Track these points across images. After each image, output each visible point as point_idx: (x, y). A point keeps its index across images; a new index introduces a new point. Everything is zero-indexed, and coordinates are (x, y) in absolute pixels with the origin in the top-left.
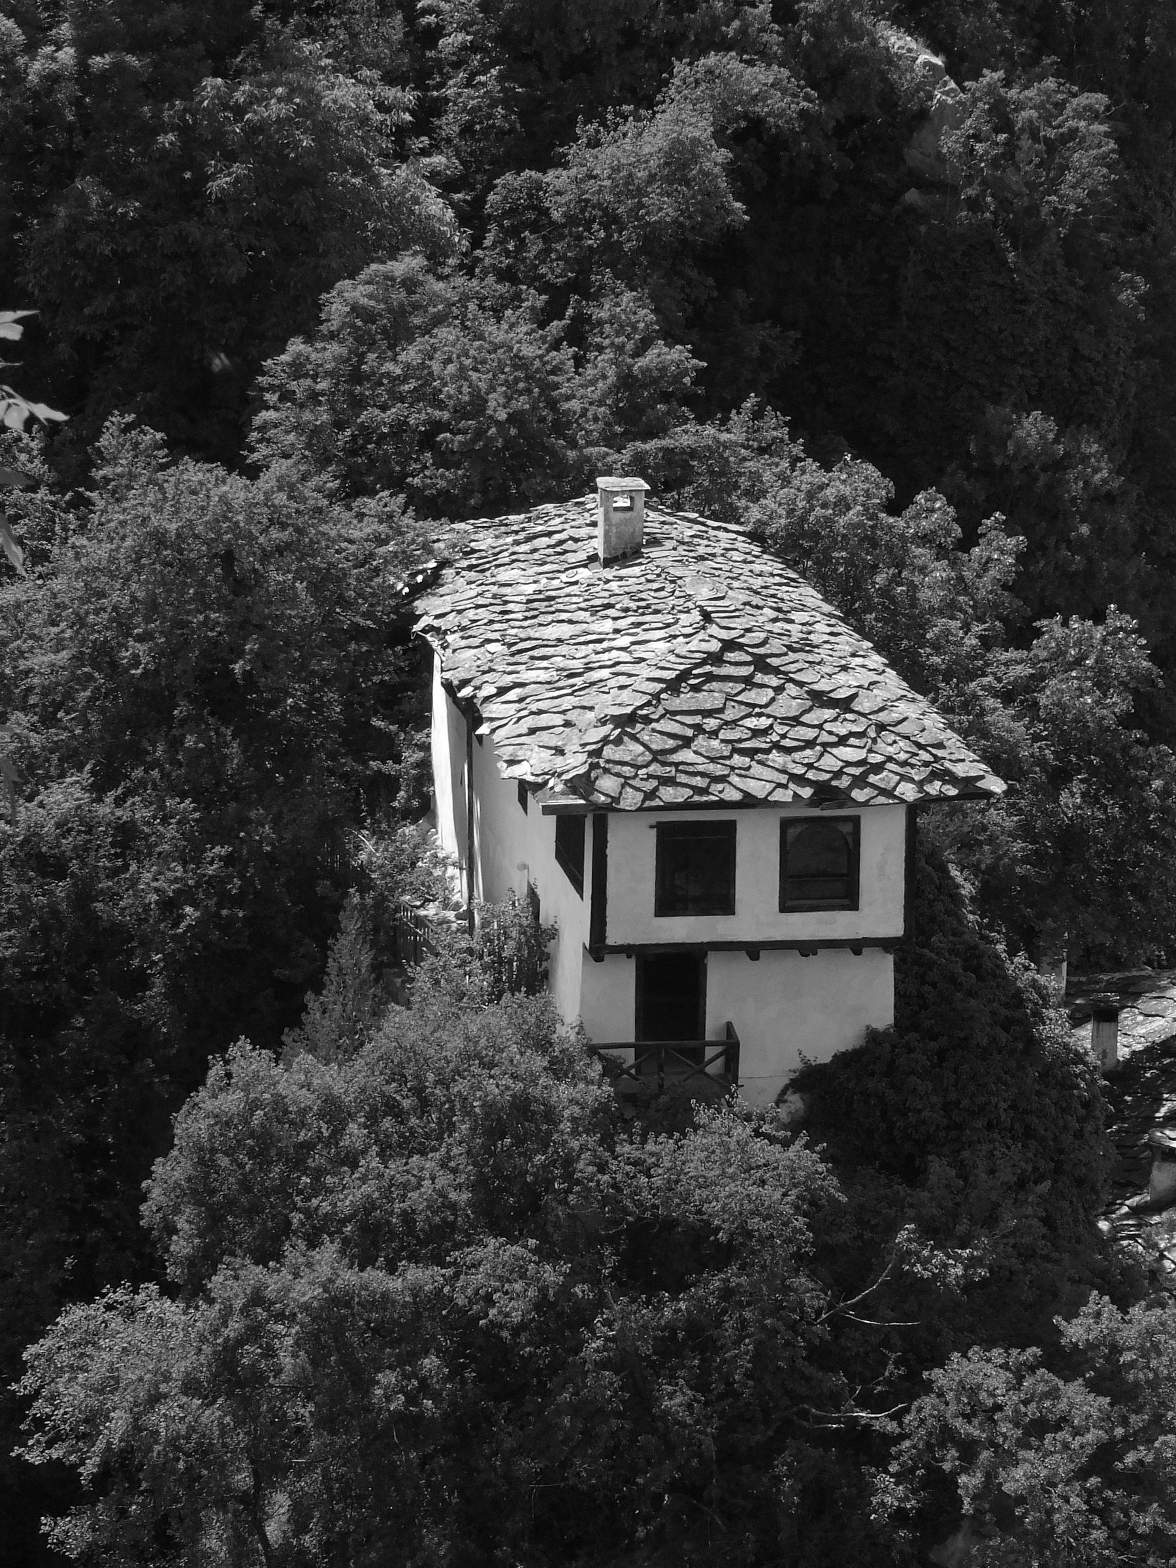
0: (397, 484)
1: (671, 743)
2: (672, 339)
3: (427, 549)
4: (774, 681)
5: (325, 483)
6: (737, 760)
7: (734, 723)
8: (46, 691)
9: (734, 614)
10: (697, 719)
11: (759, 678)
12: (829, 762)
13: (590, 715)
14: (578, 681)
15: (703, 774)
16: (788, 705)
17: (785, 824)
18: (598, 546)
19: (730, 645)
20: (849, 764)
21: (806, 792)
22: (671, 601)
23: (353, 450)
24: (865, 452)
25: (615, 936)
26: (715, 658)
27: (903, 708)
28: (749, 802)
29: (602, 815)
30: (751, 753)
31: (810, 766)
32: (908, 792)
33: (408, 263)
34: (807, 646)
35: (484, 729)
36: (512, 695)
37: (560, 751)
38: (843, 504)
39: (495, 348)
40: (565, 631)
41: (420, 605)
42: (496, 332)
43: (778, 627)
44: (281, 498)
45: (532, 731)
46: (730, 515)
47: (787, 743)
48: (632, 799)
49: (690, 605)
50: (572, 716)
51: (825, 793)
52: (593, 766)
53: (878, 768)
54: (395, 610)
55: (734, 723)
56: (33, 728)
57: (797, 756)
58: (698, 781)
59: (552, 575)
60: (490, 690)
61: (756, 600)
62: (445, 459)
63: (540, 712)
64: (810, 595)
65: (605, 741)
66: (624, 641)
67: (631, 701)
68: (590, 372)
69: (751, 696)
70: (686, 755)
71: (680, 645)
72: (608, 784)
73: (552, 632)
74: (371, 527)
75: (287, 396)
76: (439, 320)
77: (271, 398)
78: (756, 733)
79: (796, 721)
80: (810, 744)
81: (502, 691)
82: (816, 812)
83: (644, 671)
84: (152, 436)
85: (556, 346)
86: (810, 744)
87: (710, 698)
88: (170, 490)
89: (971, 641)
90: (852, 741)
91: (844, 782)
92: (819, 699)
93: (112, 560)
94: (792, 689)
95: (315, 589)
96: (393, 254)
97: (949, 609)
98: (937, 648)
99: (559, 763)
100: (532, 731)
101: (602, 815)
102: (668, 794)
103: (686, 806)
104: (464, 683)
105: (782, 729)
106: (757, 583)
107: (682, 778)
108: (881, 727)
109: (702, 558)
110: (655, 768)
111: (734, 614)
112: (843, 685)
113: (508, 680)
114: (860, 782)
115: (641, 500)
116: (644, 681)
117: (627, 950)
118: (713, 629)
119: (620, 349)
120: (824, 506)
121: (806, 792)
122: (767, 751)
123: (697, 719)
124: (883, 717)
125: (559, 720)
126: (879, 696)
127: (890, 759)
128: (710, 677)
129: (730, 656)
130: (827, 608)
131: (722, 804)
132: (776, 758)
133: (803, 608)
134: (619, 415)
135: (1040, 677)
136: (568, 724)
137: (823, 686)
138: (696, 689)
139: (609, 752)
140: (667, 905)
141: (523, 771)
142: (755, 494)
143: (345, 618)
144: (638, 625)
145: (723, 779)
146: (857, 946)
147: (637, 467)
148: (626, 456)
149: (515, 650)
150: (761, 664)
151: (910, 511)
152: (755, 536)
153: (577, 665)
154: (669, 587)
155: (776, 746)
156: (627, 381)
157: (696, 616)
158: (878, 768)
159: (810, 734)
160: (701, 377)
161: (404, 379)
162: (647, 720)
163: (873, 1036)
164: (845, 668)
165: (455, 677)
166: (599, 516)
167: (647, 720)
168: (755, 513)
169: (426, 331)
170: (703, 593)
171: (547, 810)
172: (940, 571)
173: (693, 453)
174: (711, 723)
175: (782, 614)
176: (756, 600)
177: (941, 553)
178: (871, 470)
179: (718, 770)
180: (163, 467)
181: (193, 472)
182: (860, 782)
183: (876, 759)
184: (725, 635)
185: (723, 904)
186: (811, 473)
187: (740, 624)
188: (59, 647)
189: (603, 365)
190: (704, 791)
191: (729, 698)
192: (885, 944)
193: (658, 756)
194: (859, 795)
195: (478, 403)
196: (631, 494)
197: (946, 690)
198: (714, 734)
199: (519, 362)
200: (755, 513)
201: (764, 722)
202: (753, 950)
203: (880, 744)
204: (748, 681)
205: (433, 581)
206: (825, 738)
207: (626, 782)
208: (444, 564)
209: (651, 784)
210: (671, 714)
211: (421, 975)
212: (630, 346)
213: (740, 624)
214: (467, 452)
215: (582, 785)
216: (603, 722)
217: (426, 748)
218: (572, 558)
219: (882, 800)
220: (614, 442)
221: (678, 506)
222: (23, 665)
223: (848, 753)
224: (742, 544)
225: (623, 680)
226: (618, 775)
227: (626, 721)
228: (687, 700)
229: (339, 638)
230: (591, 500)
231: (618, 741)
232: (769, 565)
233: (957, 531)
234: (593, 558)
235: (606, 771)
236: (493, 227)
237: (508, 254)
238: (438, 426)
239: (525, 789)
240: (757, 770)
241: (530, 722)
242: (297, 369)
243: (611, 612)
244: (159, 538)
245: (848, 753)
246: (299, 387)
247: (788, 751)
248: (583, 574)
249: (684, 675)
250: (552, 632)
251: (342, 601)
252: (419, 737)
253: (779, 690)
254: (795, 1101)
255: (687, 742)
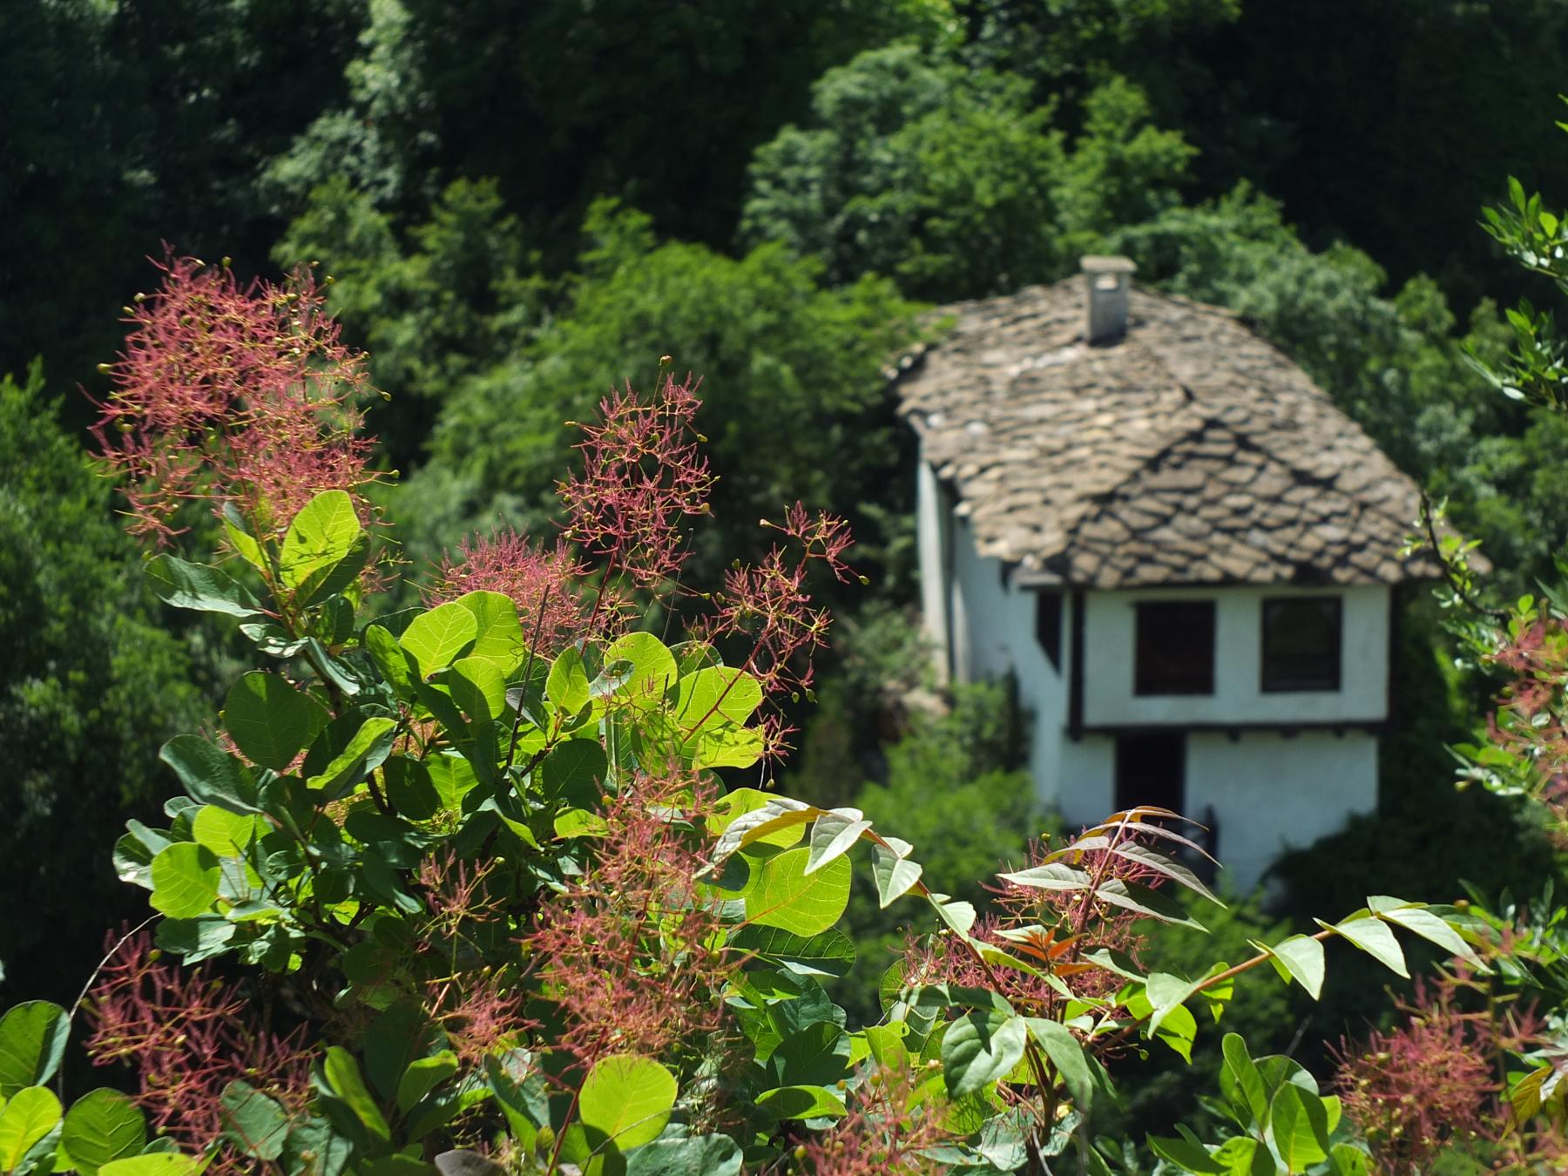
0: (885, 270)
1: (1149, 521)
2: (1163, 127)
3: (914, 334)
4: (1255, 459)
5: (974, 403)
6: (1218, 539)
7: (1213, 502)
8: (532, 472)
9: (1217, 392)
10: (1174, 498)
11: (1242, 456)
12: (1311, 541)
13: (1069, 495)
14: (1058, 460)
15: (1183, 553)
16: (1272, 481)
17: (1267, 605)
18: (1082, 327)
19: (1212, 424)
20: (1329, 543)
21: (1287, 572)
22: (1155, 381)
23: (846, 235)
24: (1359, 239)
25: (1094, 715)
26: (1196, 437)
27: (1389, 489)
28: (1229, 581)
29: (1081, 592)
30: (1231, 532)
31: (1291, 545)
32: (1391, 572)
33: (898, 52)
34: (1291, 425)
35: (963, 509)
36: (994, 474)
37: (1037, 529)
38: (1331, 289)
39: (982, 134)
40: (1047, 411)
41: (904, 390)
42: (983, 119)
43: (1263, 407)
44: (765, 282)
45: (1011, 510)
46: (1220, 300)
47: (1269, 521)
48: (1109, 577)
49: (1172, 383)
50: (1053, 494)
51: (1307, 572)
52: (1071, 544)
53: (1360, 548)
54: (883, 392)
55: (1213, 502)
56: (519, 510)
57: (1280, 534)
58: (1178, 560)
59: (1036, 356)
60: (970, 470)
61: (1241, 380)
62: (933, 244)
63: (1017, 491)
64: (1299, 378)
65: (1083, 519)
66: (1105, 419)
67: (1110, 479)
68: (1080, 158)
69: (1234, 474)
70: (1165, 534)
71: (1162, 424)
72: (1085, 563)
73: (1034, 412)
74: (859, 310)
75: (778, 183)
76: (930, 107)
77: (763, 186)
78: (1239, 512)
79: (1276, 500)
80: (1291, 523)
81: (983, 470)
82: (1296, 592)
83: (1125, 449)
84: (637, 220)
85: (1044, 130)
86: (1291, 523)
87: (1192, 476)
88: (655, 274)
89: (1462, 429)
90: (1336, 520)
91: (1326, 562)
92: (1302, 478)
93: (598, 343)
94: (1274, 468)
95: (800, 373)
96: (884, 43)
97: (1442, 395)
98: (1431, 433)
99: (1037, 541)
100: (1011, 510)
101: (1081, 592)
102: (1147, 573)
103: (1165, 584)
104: (945, 463)
105: (1261, 507)
106: (1243, 364)
107: (1161, 557)
108: (1364, 506)
109: (1187, 339)
110: (1134, 547)
111: (1217, 392)
112: (1326, 464)
113: (988, 459)
114: (1342, 561)
115: (1127, 282)
116: (1125, 458)
117: (1105, 731)
118: (1196, 408)
119: (1109, 135)
120: (1314, 289)
121: (1287, 572)
122: (1247, 530)
123: (1174, 498)
124: (1367, 496)
125: (1035, 498)
126: (1363, 475)
127: (1372, 538)
128: (1190, 456)
129: (1214, 434)
130: (1315, 391)
131: (1201, 583)
132: (1258, 537)
133: (1289, 388)
134: (1109, 202)
135: (1532, 465)
136: (1047, 502)
137: (1305, 464)
138: (1177, 467)
139: (1088, 530)
140: (1148, 683)
141: (1002, 549)
142: (1245, 279)
143: (828, 401)
144: (1119, 404)
145: (1202, 558)
146: (1339, 729)
147: (1127, 249)
148: (1115, 241)
149: (997, 431)
150: (1243, 442)
151: (1401, 299)
152: (1246, 321)
153: (1057, 444)
154: (1152, 366)
155: (1258, 525)
156: (1116, 167)
157: (1178, 395)
158: (1360, 548)
159: (1290, 512)
160: (1194, 164)
161: (893, 167)
162: (1126, 498)
163: (1356, 822)
164: (1329, 448)
165: (937, 457)
166: (1084, 297)
167: (1126, 498)
168: (1244, 297)
169: (917, 118)
170: (1186, 372)
171: (1025, 588)
172: (1430, 359)
173: (1183, 238)
174: (1191, 501)
175: (1268, 394)
176: (1241, 380)
177: (1434, 341)
178: (1360, 257)
179: (1197, 548)
180: (650, 250)
181: (677, 254)
182: (1342, 561)
183: (1358, 538)
184: (1208, 413)
185: (1200, 681)
186: (1298, 259)
187: (1221, 402)
188: (545, 427)
189: (1093, 151)
190: (1181, 569)
191: (1211, 475)
192: (1368, 728)
193: (1137, 534)
194: (1341, 575)
195: (967, 187)
196: (1118, 275)
197: (1436, 476)
198: (1193, 512)
199: (1006, 150)
200: (1244, 297)
201: (1244, 501)
202: (1234, 732)
203: (1363, 524)
204: (1230, 461)
205: (919, 364)
206: (1307, 516)
207: (1104, 560)
208: (931, 347)
209: (1128, 563)
210: (1150, 492)
211: (898, 759)
212: (1120, 133)
213: (1221, 402)
214: (956, 237)
215: (1061, 563)
216: (1081, 499)
217: (913, 533)
218: (1057, 339)
219: (1363, 580)
220: (1101, 227)
221: (1165, 292)
222: (510, 448)
223: (1332, 532)
224: (1232, 328)
225: (1103, 458)
226: (1096, 553)
227: (1105, 501)
228: (1166, 478)
229: (823, 420)
230: (1078, 283)
231: (1096, 519)
232: (1258, 351)
233: (1449, 318)
234: (1078, 339)
235: (1085, 549)
236: (990, 19)
237: (1005, 46)
238: (924, 214)
239: (1007, 568)
240: (1237, 548)
241: (1008, 501)
242: (789, 158)
243: (1095, 392)
244: (642, 322)
245: (1332, 532)
246: (789, 174)
247: (1268, 529)
248: (1070, 354)
249: (1165, 454)
250: (1034, 412)
251: (826, 384)
252: (907, 522)
253: (1261, 468)
254: (1277, 887)
255: (1165, 521)
